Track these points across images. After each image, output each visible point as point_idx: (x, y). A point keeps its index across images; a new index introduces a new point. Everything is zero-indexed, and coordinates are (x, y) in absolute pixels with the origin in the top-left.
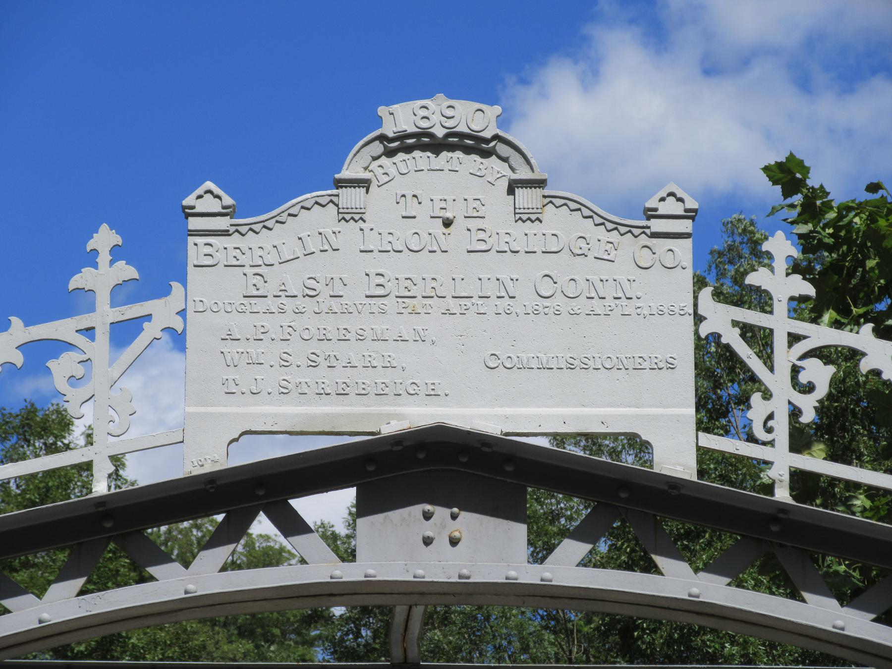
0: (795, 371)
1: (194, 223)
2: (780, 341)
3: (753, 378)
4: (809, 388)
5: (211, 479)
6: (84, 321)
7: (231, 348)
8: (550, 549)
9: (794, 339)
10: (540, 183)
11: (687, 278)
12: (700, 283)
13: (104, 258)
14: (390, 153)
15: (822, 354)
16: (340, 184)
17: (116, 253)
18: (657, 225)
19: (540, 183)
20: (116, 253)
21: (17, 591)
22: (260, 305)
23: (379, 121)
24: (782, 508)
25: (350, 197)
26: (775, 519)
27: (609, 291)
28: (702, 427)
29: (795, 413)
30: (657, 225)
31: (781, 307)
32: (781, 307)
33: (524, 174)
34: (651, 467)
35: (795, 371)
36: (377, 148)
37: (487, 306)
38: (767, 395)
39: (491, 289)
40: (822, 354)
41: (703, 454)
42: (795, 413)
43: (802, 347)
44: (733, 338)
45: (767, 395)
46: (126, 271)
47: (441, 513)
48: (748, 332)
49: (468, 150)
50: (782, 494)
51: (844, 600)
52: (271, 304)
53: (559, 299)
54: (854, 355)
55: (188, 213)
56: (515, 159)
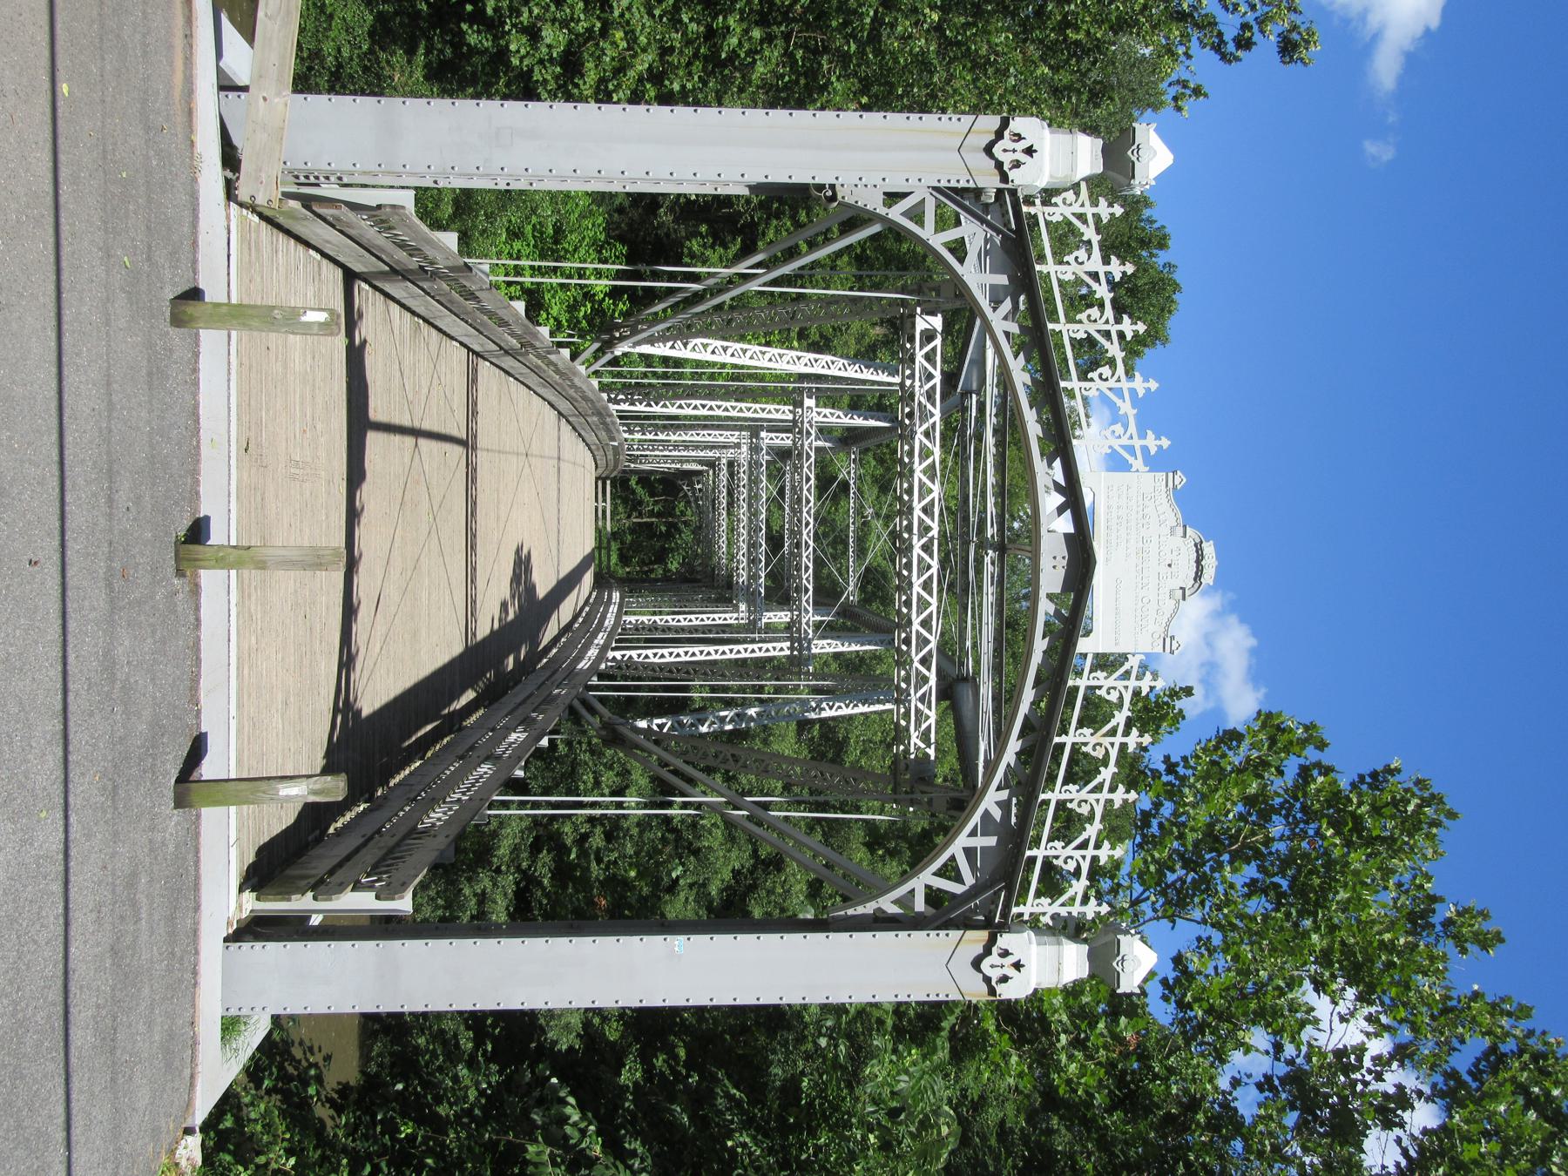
0: (1115, 688)
1: (1171, 475)
2: (1125, 683)
3: (1085, 785)
4: (1079, 806)
5: (1078, 481)
6: (1135, 436)
7: (1125, 488)
8: (1051, 600)
9: (1084, 857)
10: (1184, 599)
11: (1149, 650)
12: (1146, 655)
13: (1158, 443)
14: (1196, 545)
15: (1121, 698)
16: (1185, 527)
17: (1160, 447)
18: (1168, 640)
19: (1184, 599)
20: (1160, 447)
21: (1039, 413)
22: (1140, 498)
23: (1207, 541)
24: (1037, 798)
25: (1180, 530)
26: (1048, 733)
27: (1144, 622)
28: (1097, 656)
29: (1100, 688)
30: (1168, 640)
31: (1138, 683)
32: (1138, 683)
33: (1187, 593)
34: (1084, 636)
35: (1072, 858)
36: (1198, 541)
37: (1139, 579)
38: (1106, 678)
39: (1145, 581)
40: (1121, 698)
41: (1085, 656)
42: (1100, 688)
43: (1094, 804)
44: (1127, 666)
45: (1106, 678)
46: (1153, 451)
47: (1065, 562)
48: (1072, 899)
49: (1197, 573)
50: (1028, 853)
51: (1032, 703)
52: (1141, 502)
53: (1140, 604)
54: (1106, 766)
55: (1174, 472)
56: (1193, 590)
